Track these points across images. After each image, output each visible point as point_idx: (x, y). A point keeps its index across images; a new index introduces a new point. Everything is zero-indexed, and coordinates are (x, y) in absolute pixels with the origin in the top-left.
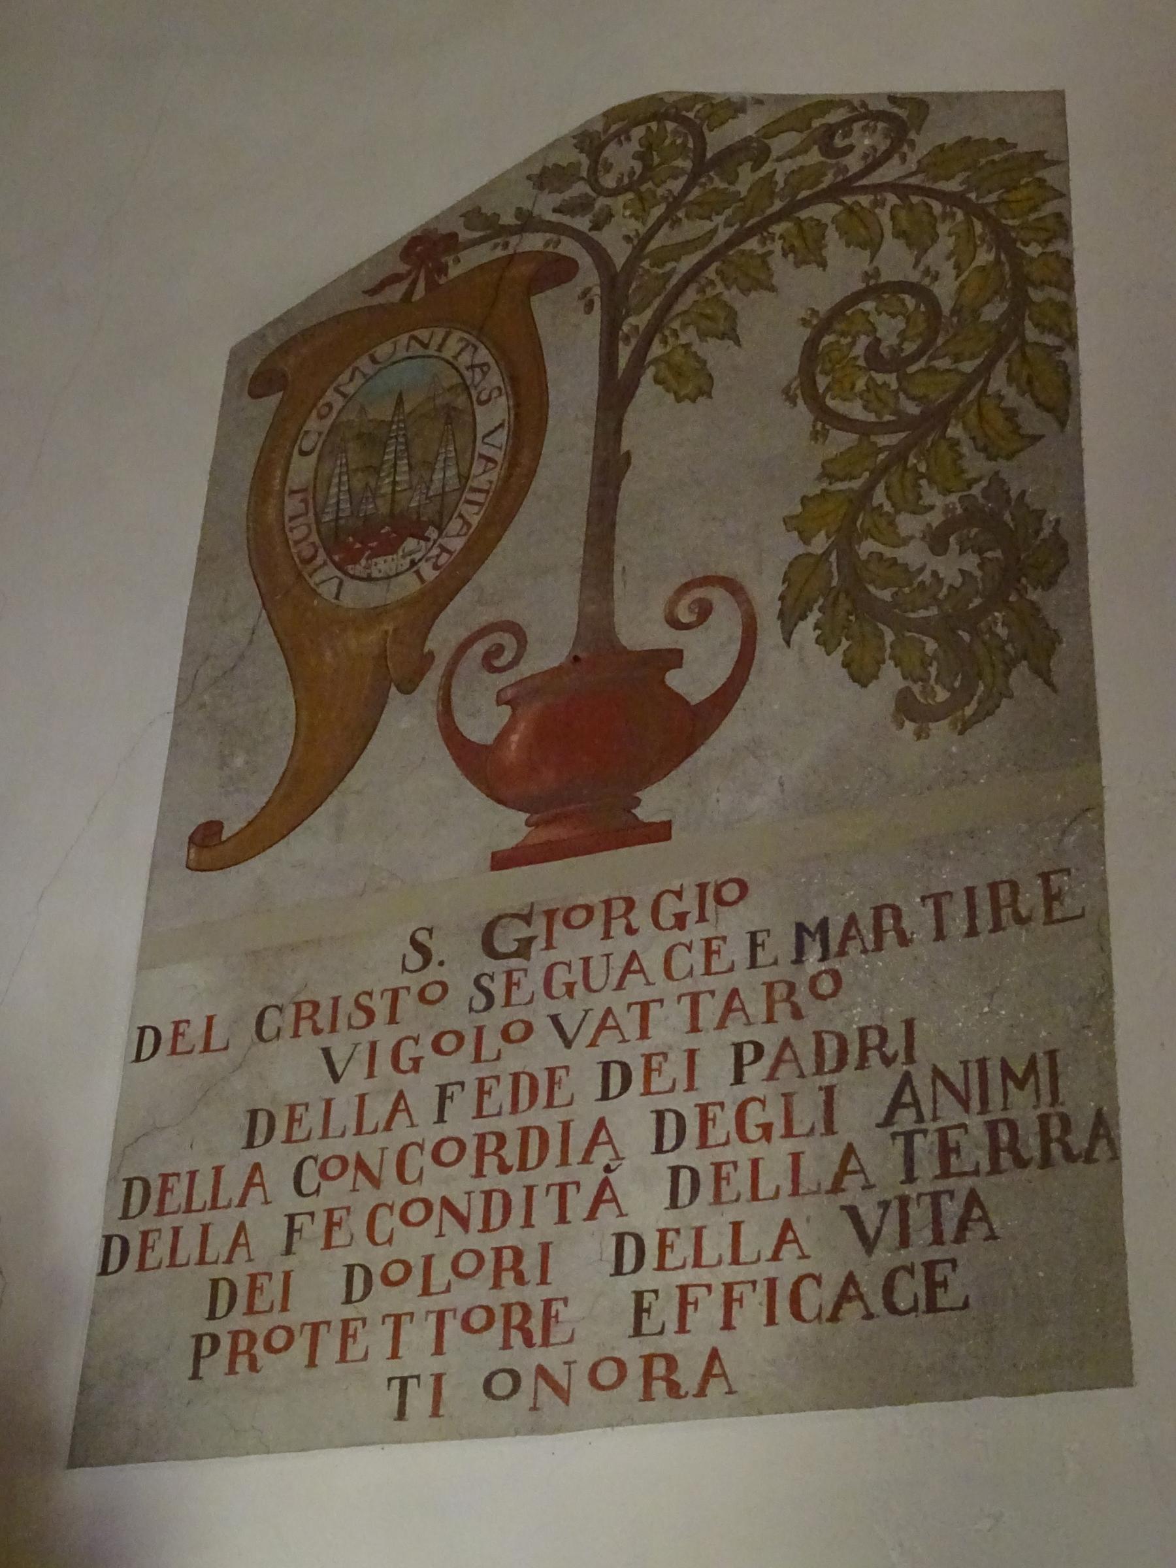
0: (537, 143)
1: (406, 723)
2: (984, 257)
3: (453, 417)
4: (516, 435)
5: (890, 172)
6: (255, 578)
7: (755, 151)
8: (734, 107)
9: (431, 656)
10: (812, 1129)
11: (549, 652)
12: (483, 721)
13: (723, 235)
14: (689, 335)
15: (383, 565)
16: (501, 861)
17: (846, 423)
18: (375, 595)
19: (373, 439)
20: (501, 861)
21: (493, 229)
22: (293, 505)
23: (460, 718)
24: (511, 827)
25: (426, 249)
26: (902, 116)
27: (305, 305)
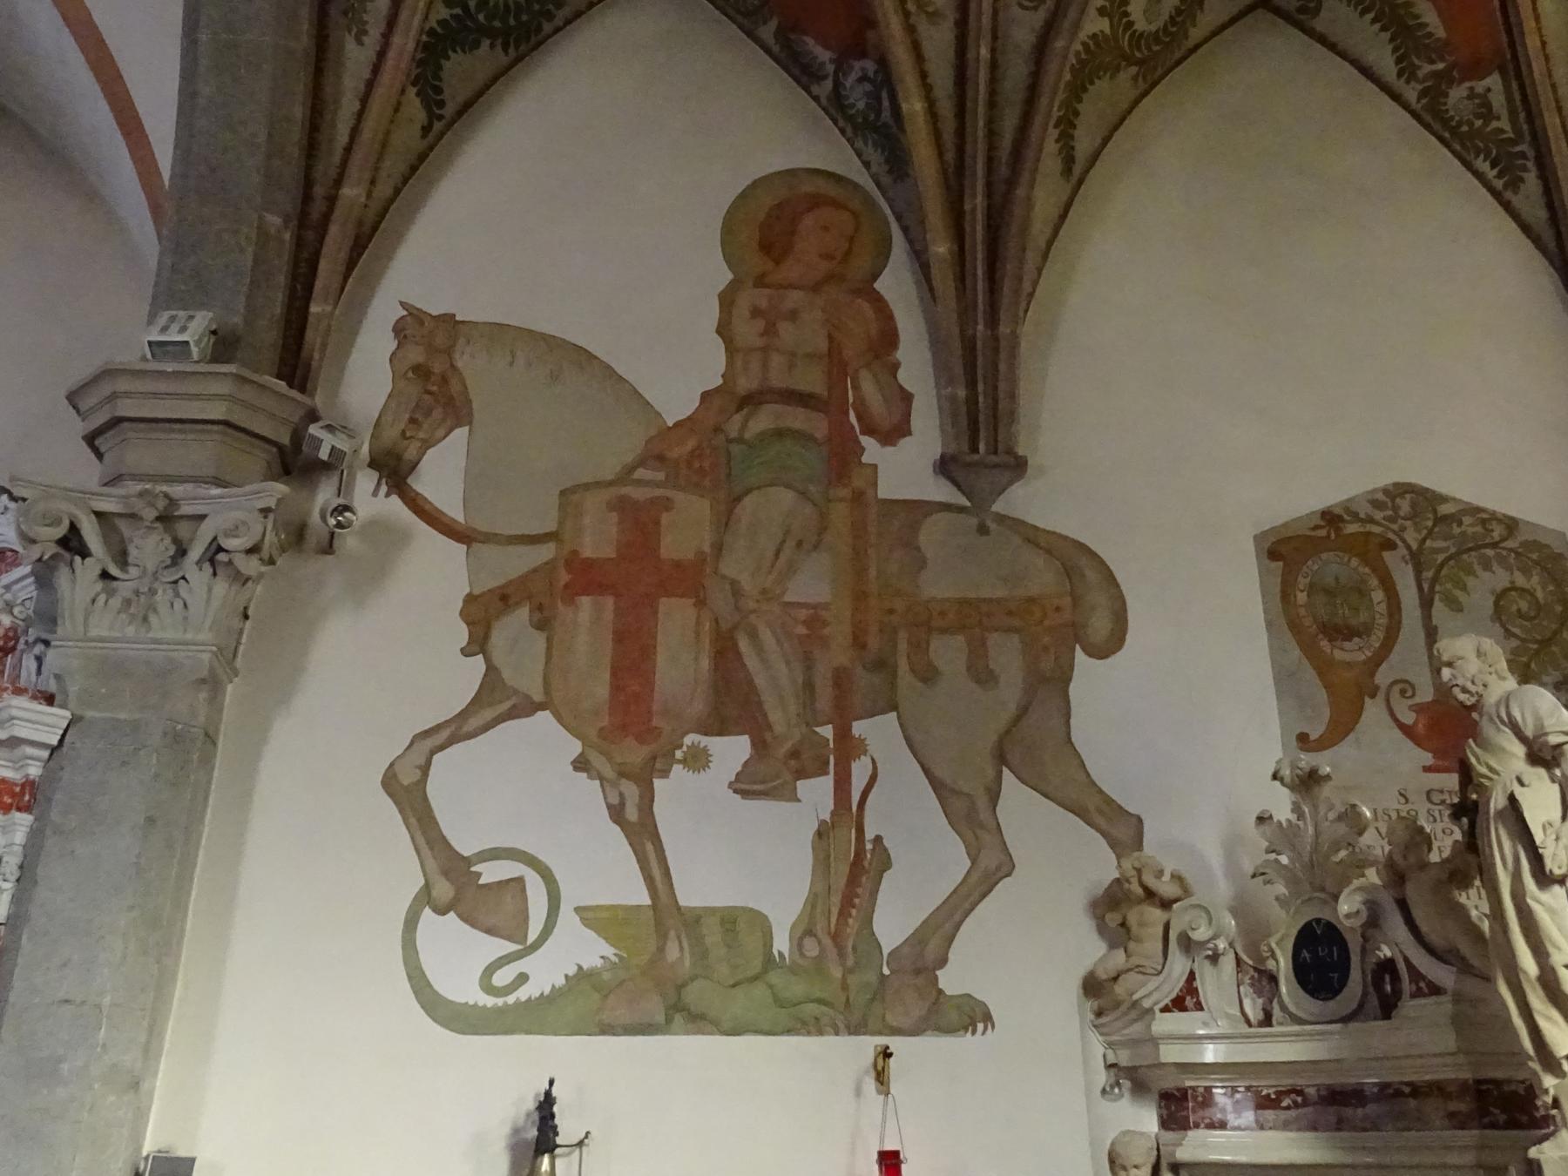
0: (1370, 487)
1: (1373, 711)
2: (1551, 588)
3: (1362, 591)
4: (1391, 615)
5: (1510, 544)
6: (1031, 295)
7: (1454, 519)
8: (1444, 499)
9: (1056, 126)
10: (1361, 1006)
11: (1426, 695)
12: (1408, 718)
13: (1453, 550)
14: (1449, 586)
15: (1347, 645)
16: (1427, 769)
17: (1515, 635)
18: (1347, 657)
19: (1329, 593)
20: (1427, 769)
21: (1355, 516)
22: (1302, 612)
23: (1400, 717)
24: (1428, 758)
25: (1330, 517)
26: (1511, 525)
27: (1285, 525)
